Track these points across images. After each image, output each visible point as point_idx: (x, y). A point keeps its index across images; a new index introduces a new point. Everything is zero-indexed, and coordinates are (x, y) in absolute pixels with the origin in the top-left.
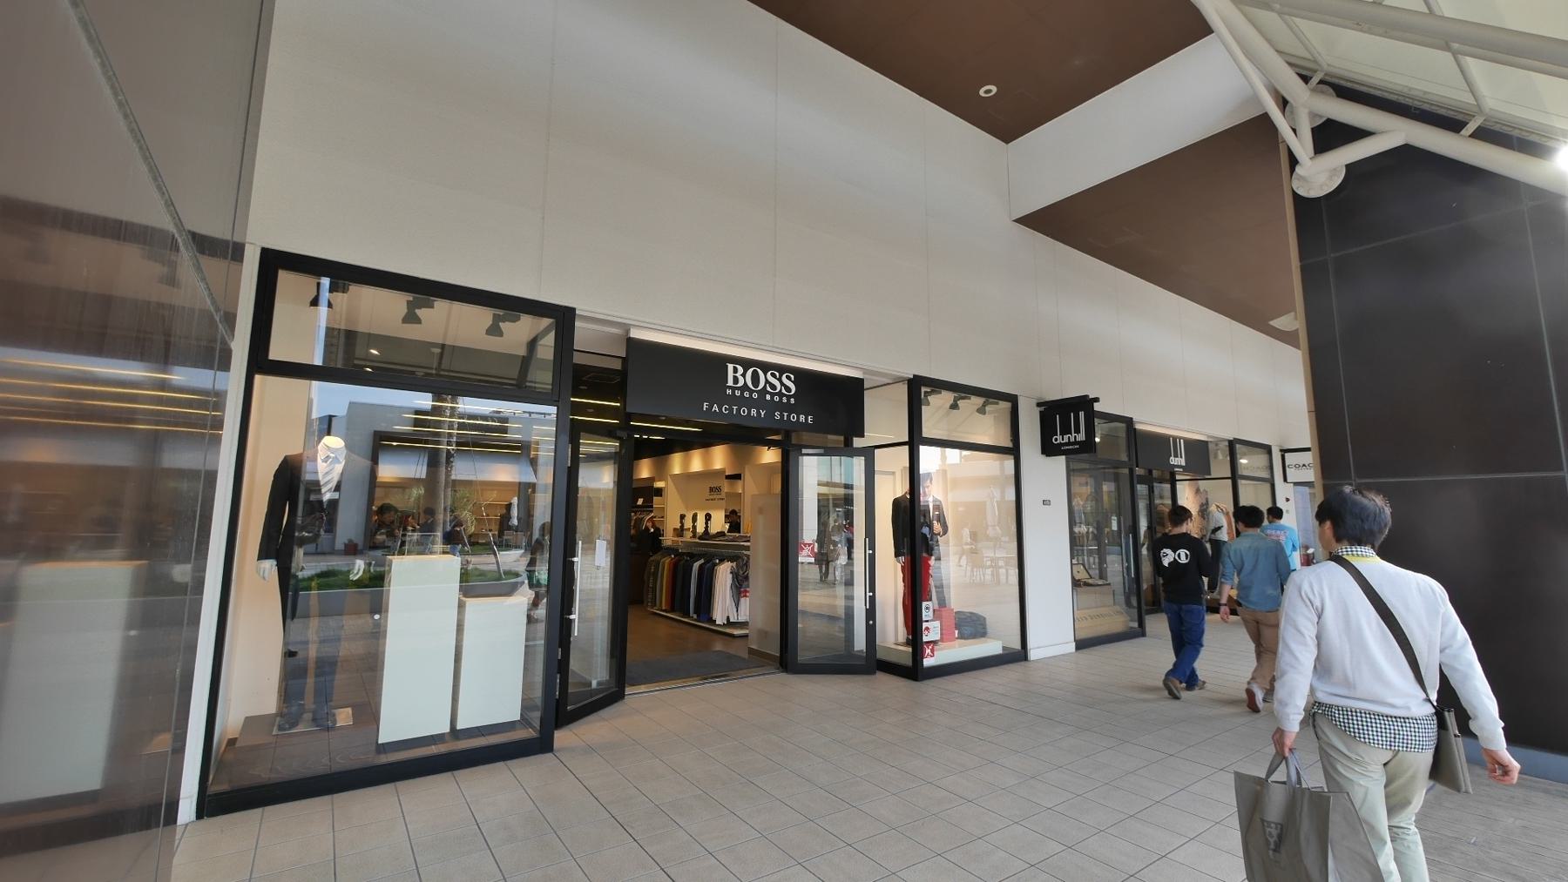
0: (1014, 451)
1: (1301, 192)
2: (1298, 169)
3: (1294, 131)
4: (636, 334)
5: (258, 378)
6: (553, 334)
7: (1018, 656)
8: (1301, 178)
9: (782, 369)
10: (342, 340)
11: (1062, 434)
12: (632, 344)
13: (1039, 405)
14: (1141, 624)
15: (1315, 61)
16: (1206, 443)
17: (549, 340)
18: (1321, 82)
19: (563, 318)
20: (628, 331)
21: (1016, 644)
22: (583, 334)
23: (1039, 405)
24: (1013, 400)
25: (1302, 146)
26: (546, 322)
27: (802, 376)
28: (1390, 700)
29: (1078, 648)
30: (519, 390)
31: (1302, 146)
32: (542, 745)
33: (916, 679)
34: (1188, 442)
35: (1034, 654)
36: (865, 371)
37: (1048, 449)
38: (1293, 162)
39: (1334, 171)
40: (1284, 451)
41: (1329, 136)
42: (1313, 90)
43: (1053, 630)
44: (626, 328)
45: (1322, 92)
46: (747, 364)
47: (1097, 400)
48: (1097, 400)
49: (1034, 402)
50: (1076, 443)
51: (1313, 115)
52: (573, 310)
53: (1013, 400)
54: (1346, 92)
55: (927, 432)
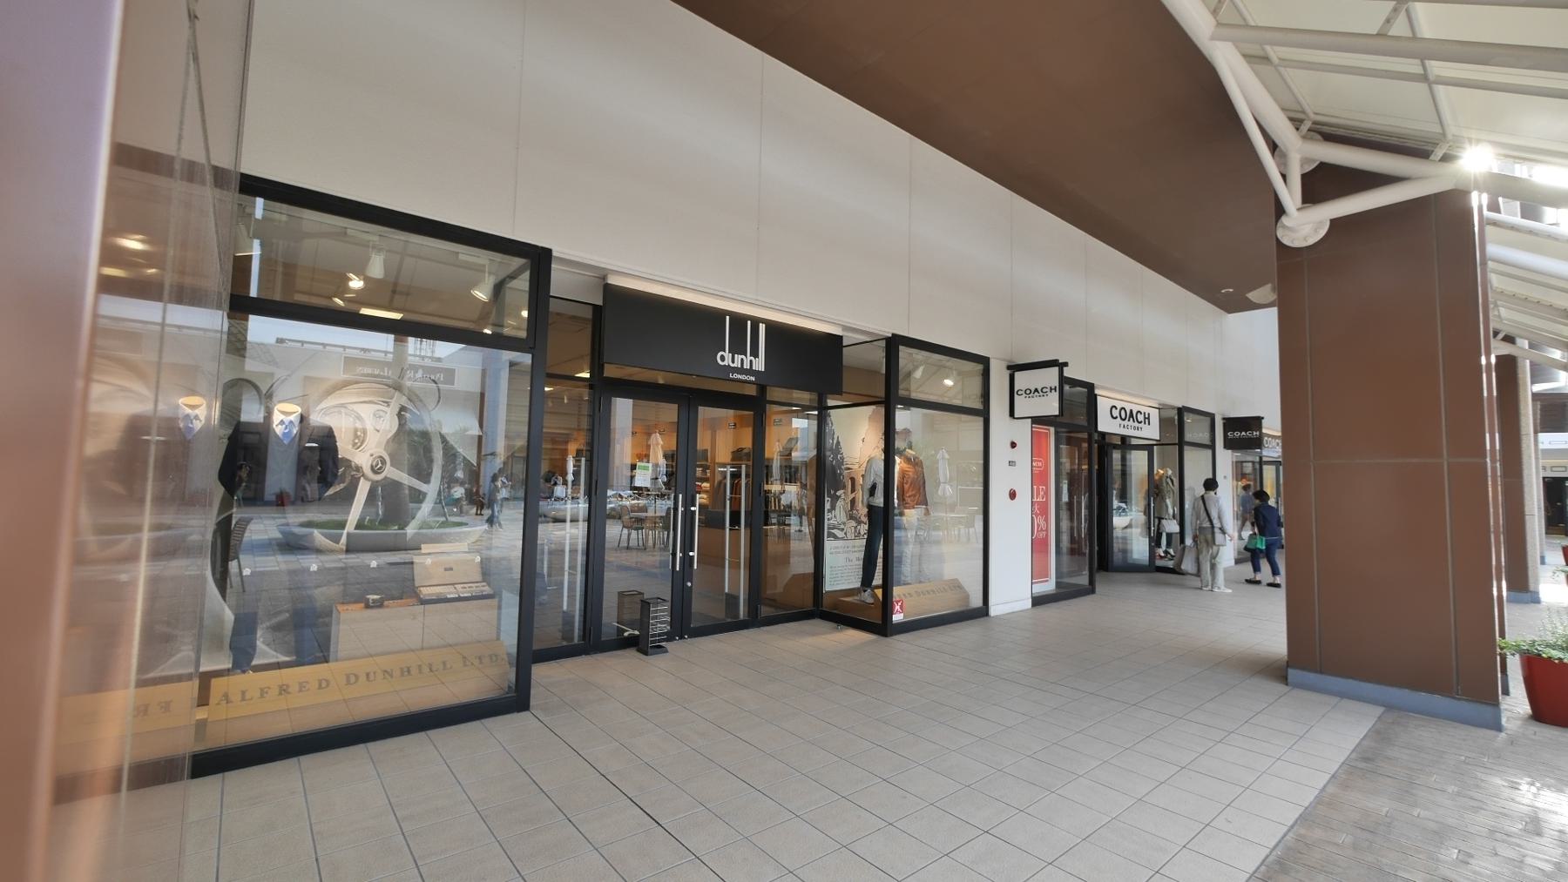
1: (1286, 241)
2: (1284, 219)
3: (1284, 176)
4: (614, 280)
6: (527, 275)
7: (983, 612)
8: (1284, 227)
10: (280, 269)
11: (733, 351)
12: (609, 291)
14: (1092, 582)
15: (1303, 112)
16: (836, 340)
17: (523, 283)
19: (539, 259)
20: (604, 278)
21: (976, 601)
22: (561, 282)
24: (984, 361)
25: (1290, 196)
26: (517, 262)
29: (1034, 604)
30: (187, 295)
31: (1290, 196)
32: (516, 700)
33: (885, 635)
34: (775, 330)
35: (994, 610)
36: (846, 328)
38: (1280, 211)
40: (1014, 368)
42: (1304, 137)
43: (1013, 589)
44: (602, 275)
45: (1311, 139)
49: (1004, 365)
50: (750, 372)
52: (549, 251)
55: (1188, 437)
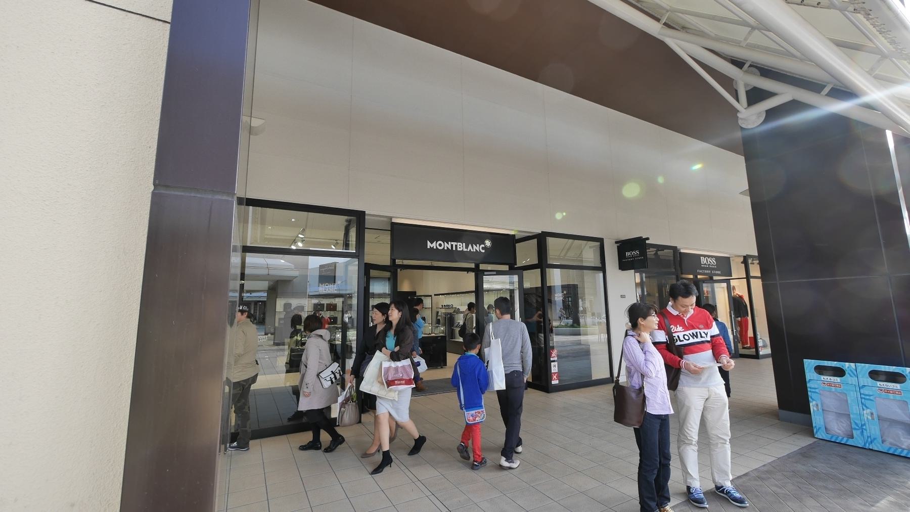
0: (602, 268)
4: (394, 220)
5: (540, 285)
9: (712, 257)
13: (616, 242)
18: (751, 66)
23: (616, 242)
24: (601, 241)
27: (717, 258)
28: (518, 349)
37: (624, 265)
39: (759, 114)
41: (756, 96)
46: (705, 256)
47: (648, 239)
48: (648, 239)
51: (746, 85)
52: (640, 238)
53: (601, 241)
54: (766, 72)
